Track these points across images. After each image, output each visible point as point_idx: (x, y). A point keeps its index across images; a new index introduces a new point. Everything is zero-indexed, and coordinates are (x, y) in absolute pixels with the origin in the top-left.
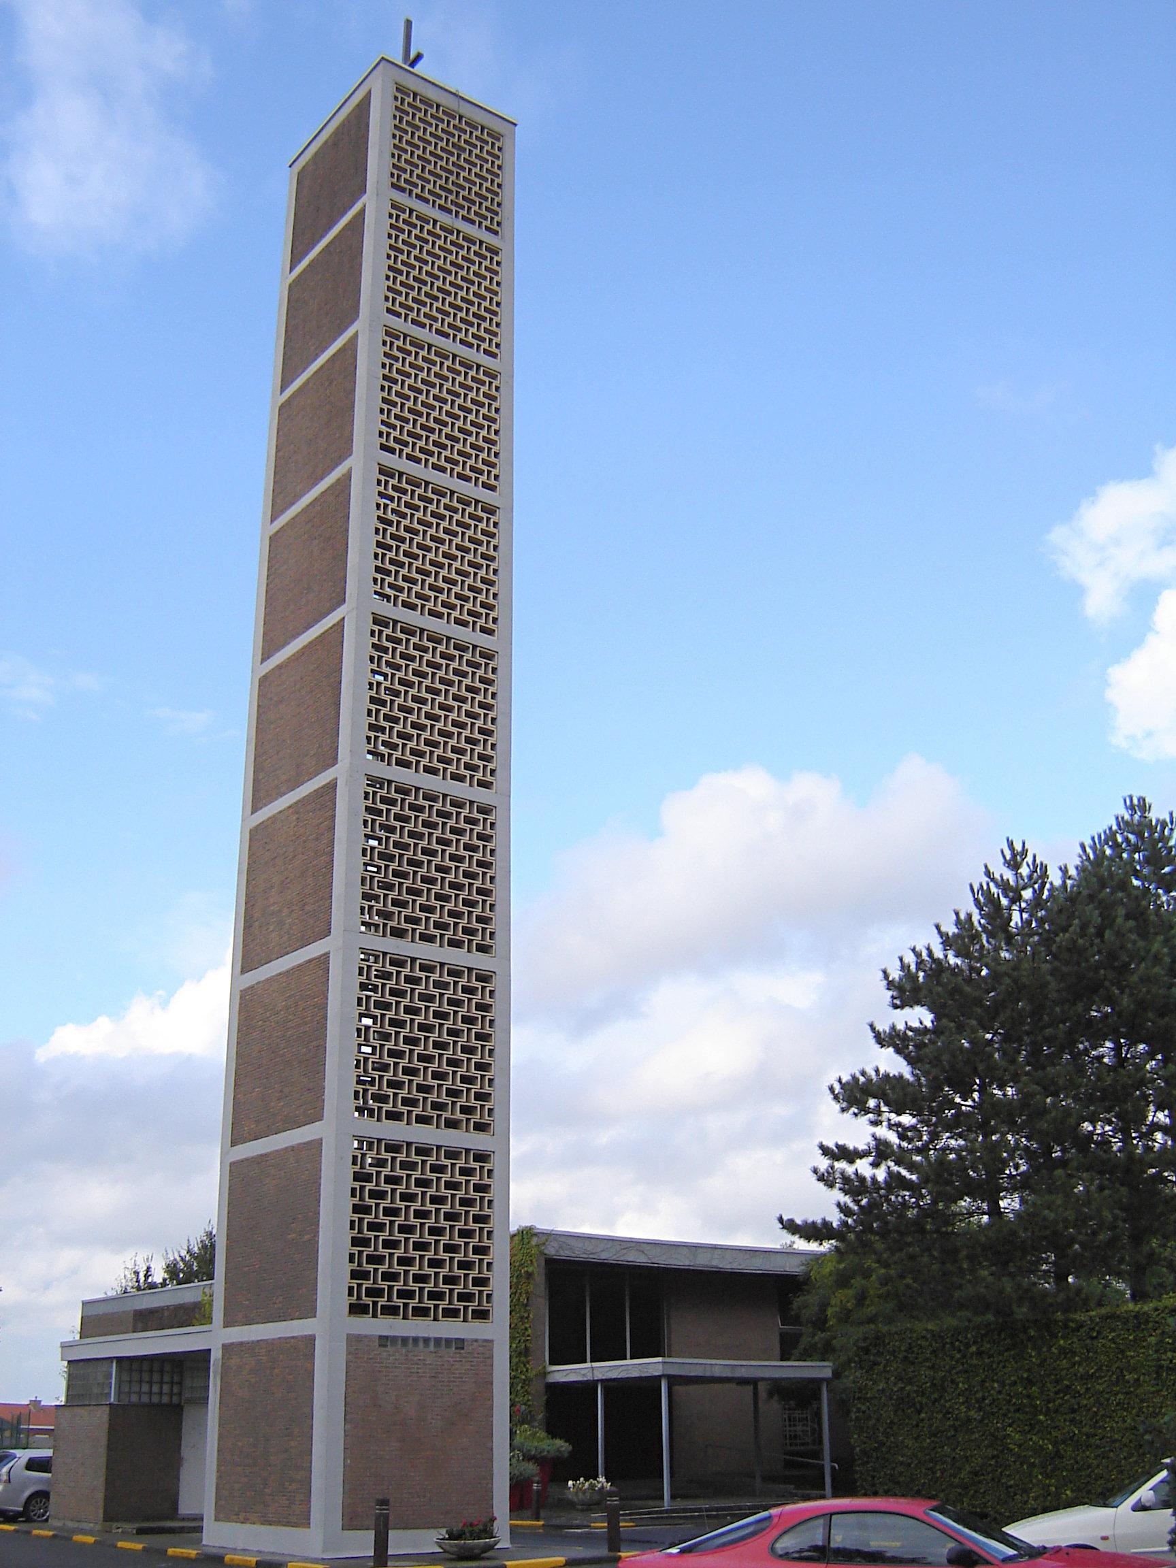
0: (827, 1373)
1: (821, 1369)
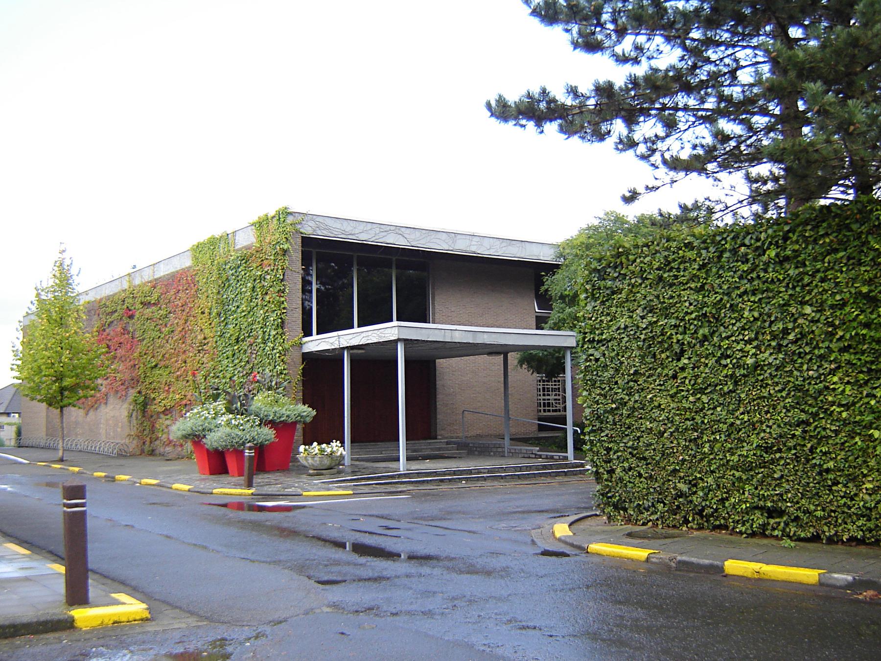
0: (572, 342)
1: (566, 338)
